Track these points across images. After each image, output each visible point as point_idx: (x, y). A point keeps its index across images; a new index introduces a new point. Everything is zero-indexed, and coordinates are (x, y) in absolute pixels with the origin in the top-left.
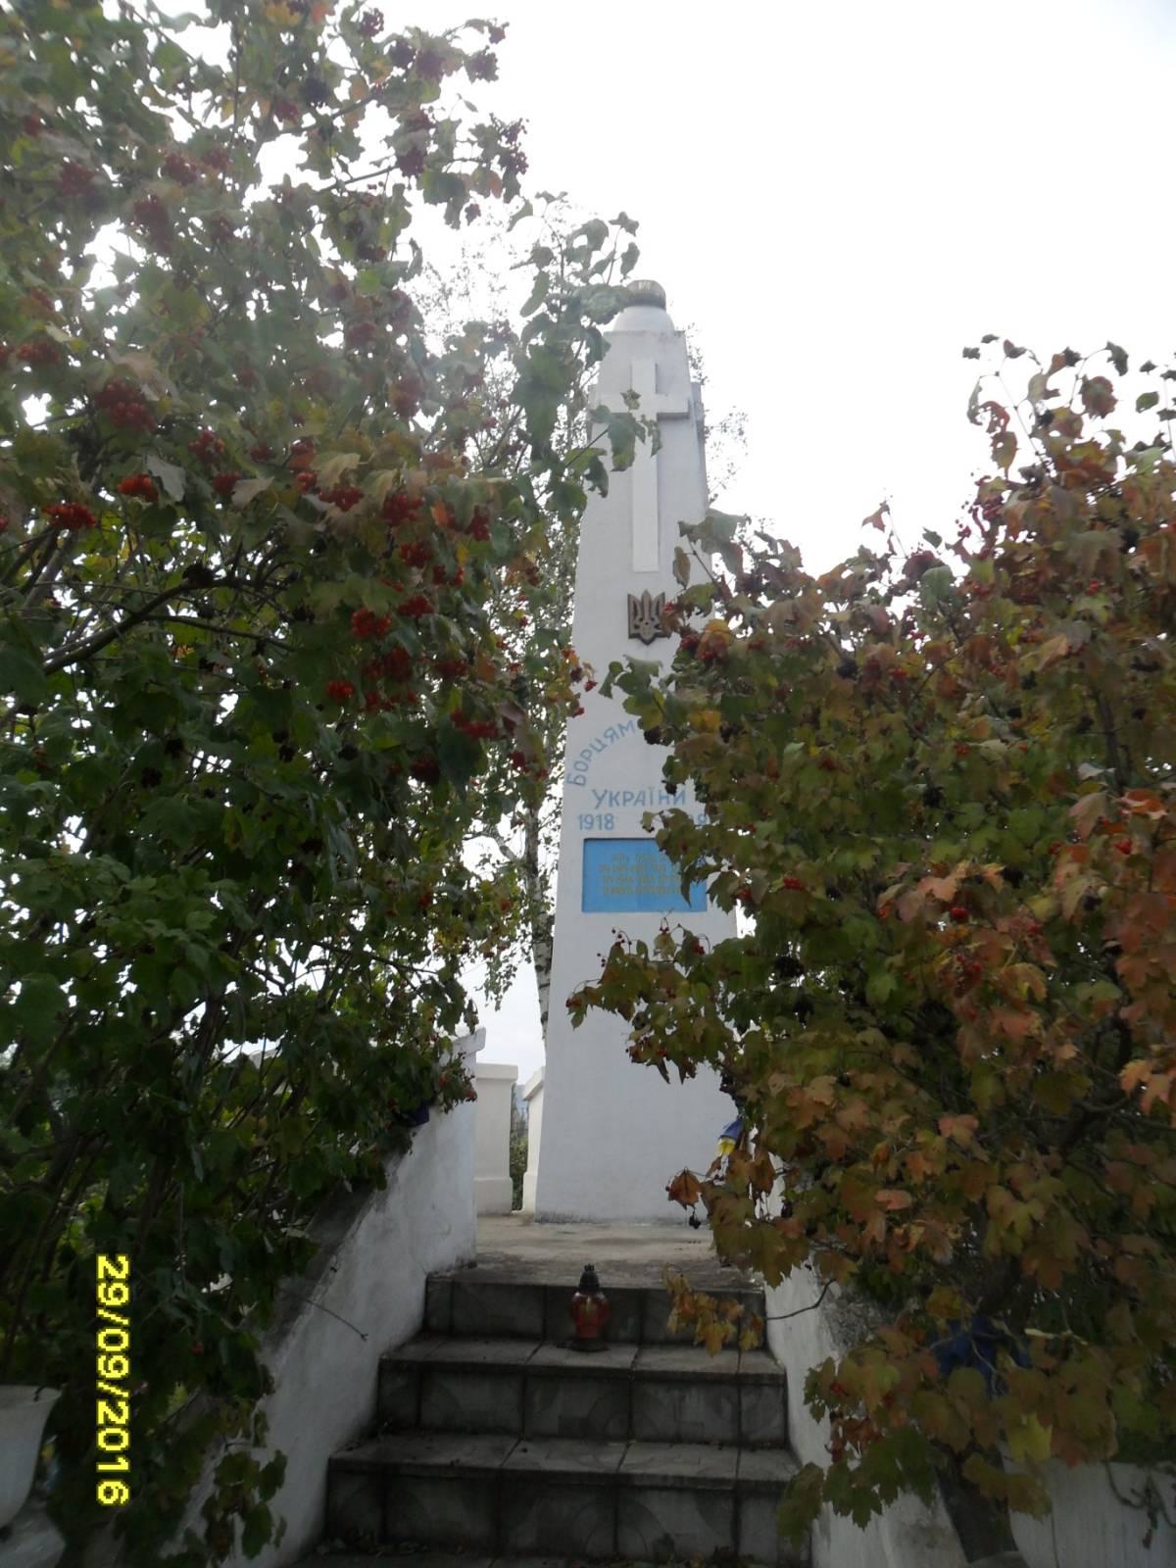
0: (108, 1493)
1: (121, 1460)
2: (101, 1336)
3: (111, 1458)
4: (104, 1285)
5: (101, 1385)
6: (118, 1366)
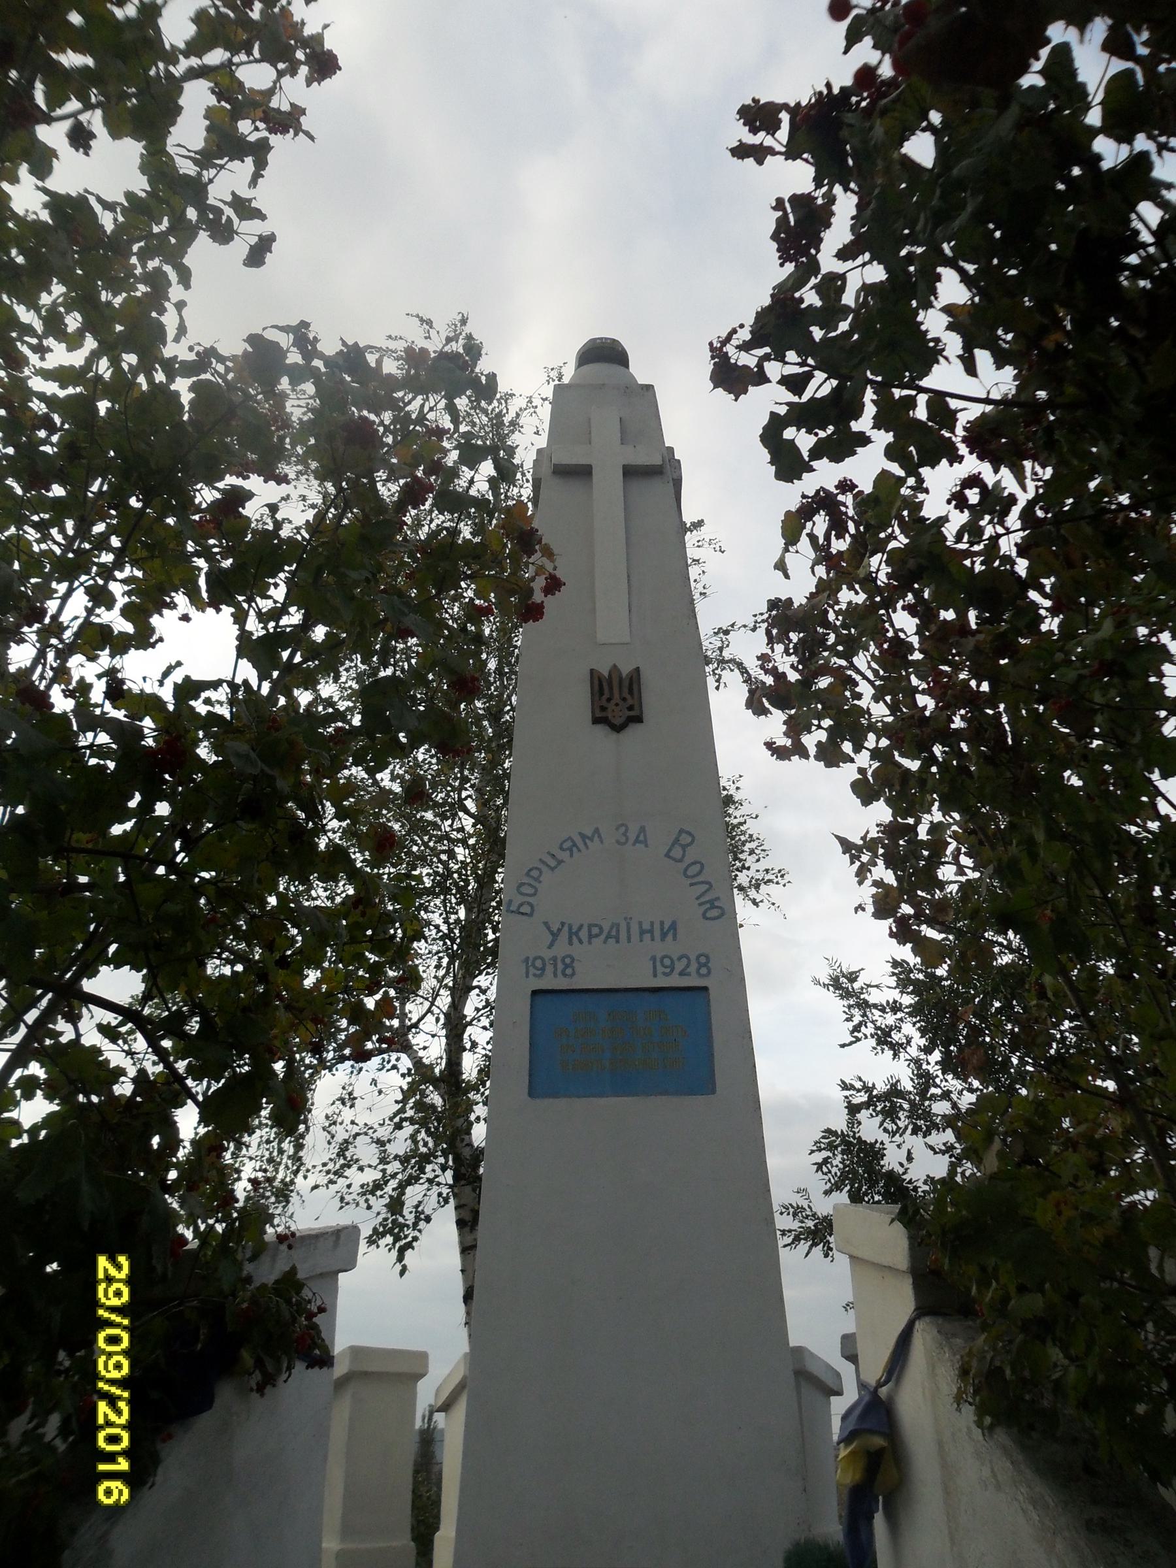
0: (108, 1493)
1: (120, 1459)
2: (101, 1336)
3: (111, 1458)
4: (103, 1285)
5: (101, 1385)
6: (118, 1366)
